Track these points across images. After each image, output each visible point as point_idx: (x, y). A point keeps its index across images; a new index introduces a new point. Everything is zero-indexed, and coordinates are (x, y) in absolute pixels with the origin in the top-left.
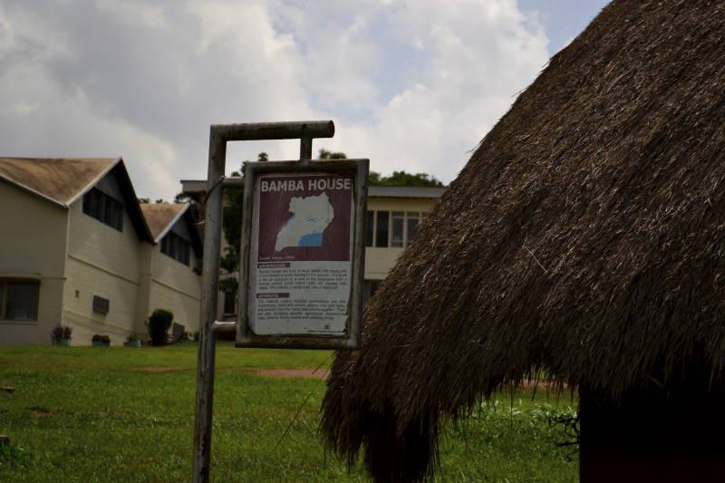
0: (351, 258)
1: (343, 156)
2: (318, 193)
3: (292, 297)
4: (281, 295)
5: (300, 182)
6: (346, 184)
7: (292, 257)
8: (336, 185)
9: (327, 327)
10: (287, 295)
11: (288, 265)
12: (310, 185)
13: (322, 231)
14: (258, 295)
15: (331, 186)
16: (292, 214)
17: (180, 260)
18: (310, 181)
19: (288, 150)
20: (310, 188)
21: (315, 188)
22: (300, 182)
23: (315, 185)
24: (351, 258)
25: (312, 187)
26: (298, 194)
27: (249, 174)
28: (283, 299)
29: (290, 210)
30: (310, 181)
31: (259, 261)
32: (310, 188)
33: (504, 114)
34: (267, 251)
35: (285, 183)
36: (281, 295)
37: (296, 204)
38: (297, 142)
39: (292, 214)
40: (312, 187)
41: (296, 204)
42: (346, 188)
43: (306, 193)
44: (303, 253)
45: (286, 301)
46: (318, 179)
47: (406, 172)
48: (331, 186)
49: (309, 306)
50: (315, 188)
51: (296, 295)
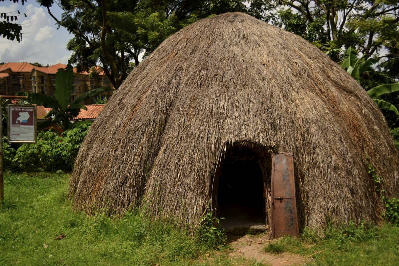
2: (26, 112)
16: (20, 116)
37: (21, 114)
41: (21, 114)
44: (23, 124)
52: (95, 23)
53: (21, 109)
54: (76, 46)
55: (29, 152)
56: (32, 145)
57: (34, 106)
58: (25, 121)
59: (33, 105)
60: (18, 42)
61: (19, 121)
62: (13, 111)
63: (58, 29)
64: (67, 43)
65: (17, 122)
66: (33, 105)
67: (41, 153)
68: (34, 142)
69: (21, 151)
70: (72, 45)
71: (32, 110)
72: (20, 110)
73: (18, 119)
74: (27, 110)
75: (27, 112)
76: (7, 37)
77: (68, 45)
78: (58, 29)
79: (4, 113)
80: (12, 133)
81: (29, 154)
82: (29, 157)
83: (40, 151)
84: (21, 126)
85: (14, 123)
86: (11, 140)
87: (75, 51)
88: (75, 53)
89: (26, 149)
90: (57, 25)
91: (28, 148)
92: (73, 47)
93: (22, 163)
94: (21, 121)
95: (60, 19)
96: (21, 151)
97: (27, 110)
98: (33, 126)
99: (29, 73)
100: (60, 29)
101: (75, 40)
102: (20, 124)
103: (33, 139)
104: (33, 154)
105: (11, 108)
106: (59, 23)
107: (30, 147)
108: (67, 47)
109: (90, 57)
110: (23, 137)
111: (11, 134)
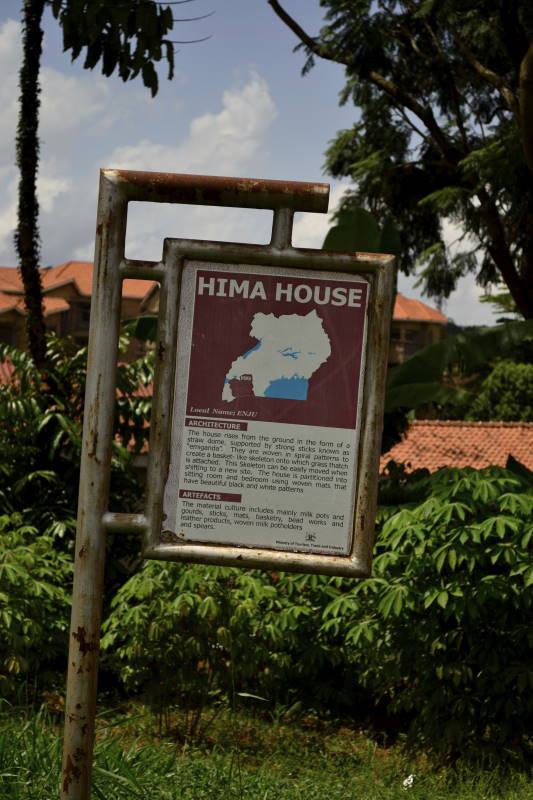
0: (358, 424)
1: (277, 316)
2: (303, 310)
3: (244, 502)
4: (226, 497)
5: (259, 285)
6: (352, 297)
7: (252, 414)
8: (332, 298)
9: (310, 538)
10: (237, 498)
11: (244, 427)
12: (279, 291)
13: (308, 376)
14: (182, 492)
15: (322, 297)
16: (254, 343)
17: (86, 361)
18: (279, 286)
19: (251, 226)
20: (278, 298)
21: (289, 299)
22: (259, 285)
23: (289, 292)
24: (358, 424)
25: (284, 296)
26: (260, 306)
27: (172, 259)
28: (230, 504)
29: (252, 334)
30: (279, 286)
31: (188, 413)
32: (278, 298)
33: (135, 281)
34: (204, 396)
35: (246, 284)
36: (226, 497)
37: (262, 325)
38: (268, 215)
39: (254, 343)
40: (284, 296)
41: (262, 325)
42: (351, 304)
43: (280, 308)
44: (278, 409)
45: (233, 508)
46: (296, 282)
47: (40, 109)
48: (322, 297)
49: (288, 476)
50: (289, 299)
51: (251, 498)
52: (483, 29)
53: (270, 284)
54: (367, 155)
55: (175, 607)
56: (190, 574)
57: (369, 271)
58: (294, 382)
59: (363, 257)
60: (149, 91)
61: (244, 386)
62: (203, 301)
63: (305, 70)
64: (327, 147)
65: (227, 395)
66: (363, 257)
67: (233, 619)
68: (352, 563)
69: (133, 602)
70: (348, 153)
71: (352, 299)
72: (260, 290)
73: (238, 368)
74: (313, 294)
75: (313, 320)
76: (100, 64)
77: (329, 153)
78: (305, 70)
79: (65, 413)
80: (182, 475)
81: (170, 617)
82: (172, 632)
83: (226, 608)
84: (257, 428)
85: (204, 396)
86: (172, 538)
87: (355, 177)
88: (355, 187)
89: (156, 592)
90: (302, 56)
91: (170, 589)
92: (352, 161)
93: (135, 662)
94: (259, 390)
95: (313, 32)
96: (133, 602)
97: (313, 294)
98: (348, 437)
99: (139, 300)
100: (313, 71)
101: (362, 132)
102: (253, 406)
103: (343, 542)
104: (189, 622)
105: (191, 270)
106: (309, 43)
107: (181, 585)
108: (324, 160)
109: (432, 196)
110: (266, 518)
111: (171, 491)
